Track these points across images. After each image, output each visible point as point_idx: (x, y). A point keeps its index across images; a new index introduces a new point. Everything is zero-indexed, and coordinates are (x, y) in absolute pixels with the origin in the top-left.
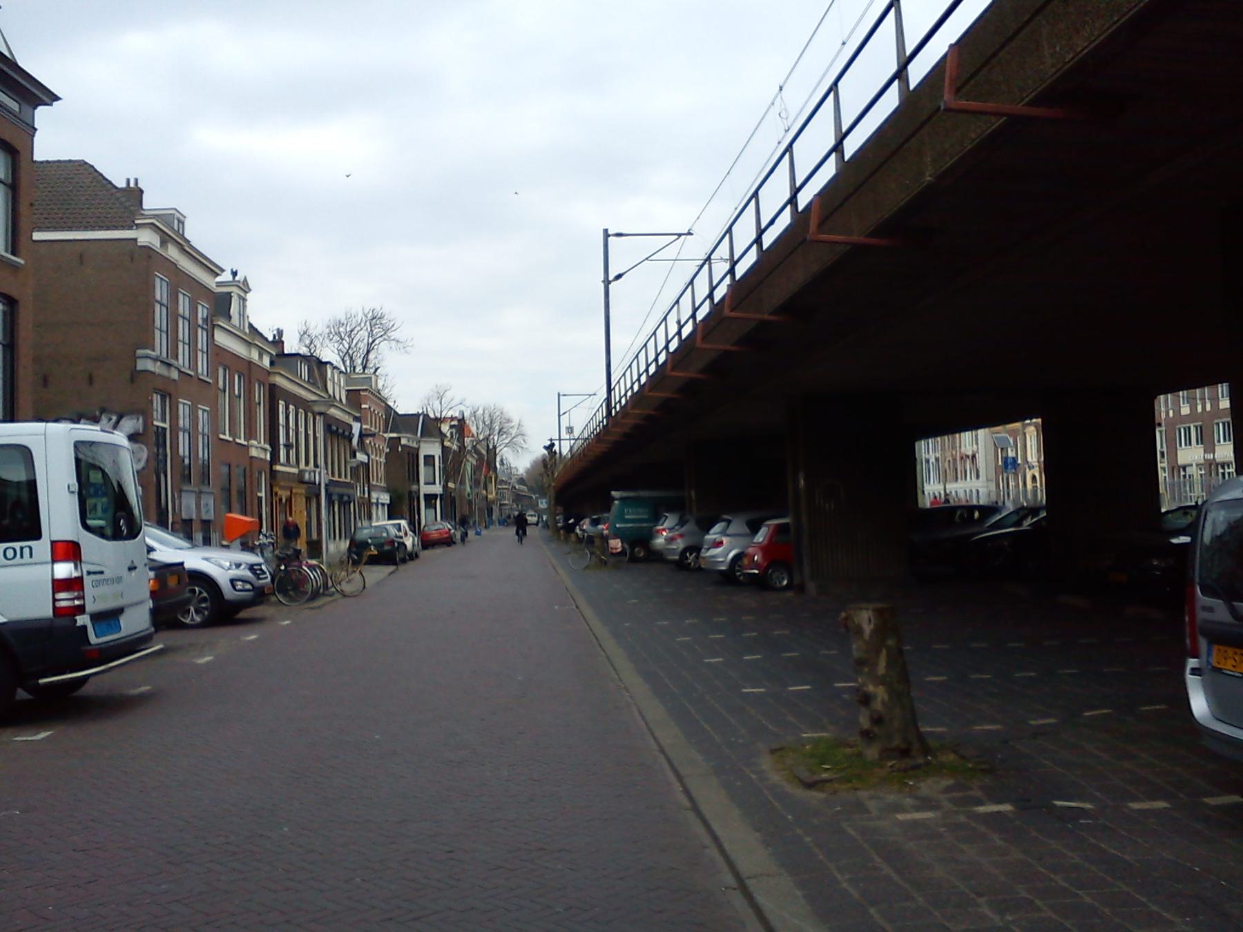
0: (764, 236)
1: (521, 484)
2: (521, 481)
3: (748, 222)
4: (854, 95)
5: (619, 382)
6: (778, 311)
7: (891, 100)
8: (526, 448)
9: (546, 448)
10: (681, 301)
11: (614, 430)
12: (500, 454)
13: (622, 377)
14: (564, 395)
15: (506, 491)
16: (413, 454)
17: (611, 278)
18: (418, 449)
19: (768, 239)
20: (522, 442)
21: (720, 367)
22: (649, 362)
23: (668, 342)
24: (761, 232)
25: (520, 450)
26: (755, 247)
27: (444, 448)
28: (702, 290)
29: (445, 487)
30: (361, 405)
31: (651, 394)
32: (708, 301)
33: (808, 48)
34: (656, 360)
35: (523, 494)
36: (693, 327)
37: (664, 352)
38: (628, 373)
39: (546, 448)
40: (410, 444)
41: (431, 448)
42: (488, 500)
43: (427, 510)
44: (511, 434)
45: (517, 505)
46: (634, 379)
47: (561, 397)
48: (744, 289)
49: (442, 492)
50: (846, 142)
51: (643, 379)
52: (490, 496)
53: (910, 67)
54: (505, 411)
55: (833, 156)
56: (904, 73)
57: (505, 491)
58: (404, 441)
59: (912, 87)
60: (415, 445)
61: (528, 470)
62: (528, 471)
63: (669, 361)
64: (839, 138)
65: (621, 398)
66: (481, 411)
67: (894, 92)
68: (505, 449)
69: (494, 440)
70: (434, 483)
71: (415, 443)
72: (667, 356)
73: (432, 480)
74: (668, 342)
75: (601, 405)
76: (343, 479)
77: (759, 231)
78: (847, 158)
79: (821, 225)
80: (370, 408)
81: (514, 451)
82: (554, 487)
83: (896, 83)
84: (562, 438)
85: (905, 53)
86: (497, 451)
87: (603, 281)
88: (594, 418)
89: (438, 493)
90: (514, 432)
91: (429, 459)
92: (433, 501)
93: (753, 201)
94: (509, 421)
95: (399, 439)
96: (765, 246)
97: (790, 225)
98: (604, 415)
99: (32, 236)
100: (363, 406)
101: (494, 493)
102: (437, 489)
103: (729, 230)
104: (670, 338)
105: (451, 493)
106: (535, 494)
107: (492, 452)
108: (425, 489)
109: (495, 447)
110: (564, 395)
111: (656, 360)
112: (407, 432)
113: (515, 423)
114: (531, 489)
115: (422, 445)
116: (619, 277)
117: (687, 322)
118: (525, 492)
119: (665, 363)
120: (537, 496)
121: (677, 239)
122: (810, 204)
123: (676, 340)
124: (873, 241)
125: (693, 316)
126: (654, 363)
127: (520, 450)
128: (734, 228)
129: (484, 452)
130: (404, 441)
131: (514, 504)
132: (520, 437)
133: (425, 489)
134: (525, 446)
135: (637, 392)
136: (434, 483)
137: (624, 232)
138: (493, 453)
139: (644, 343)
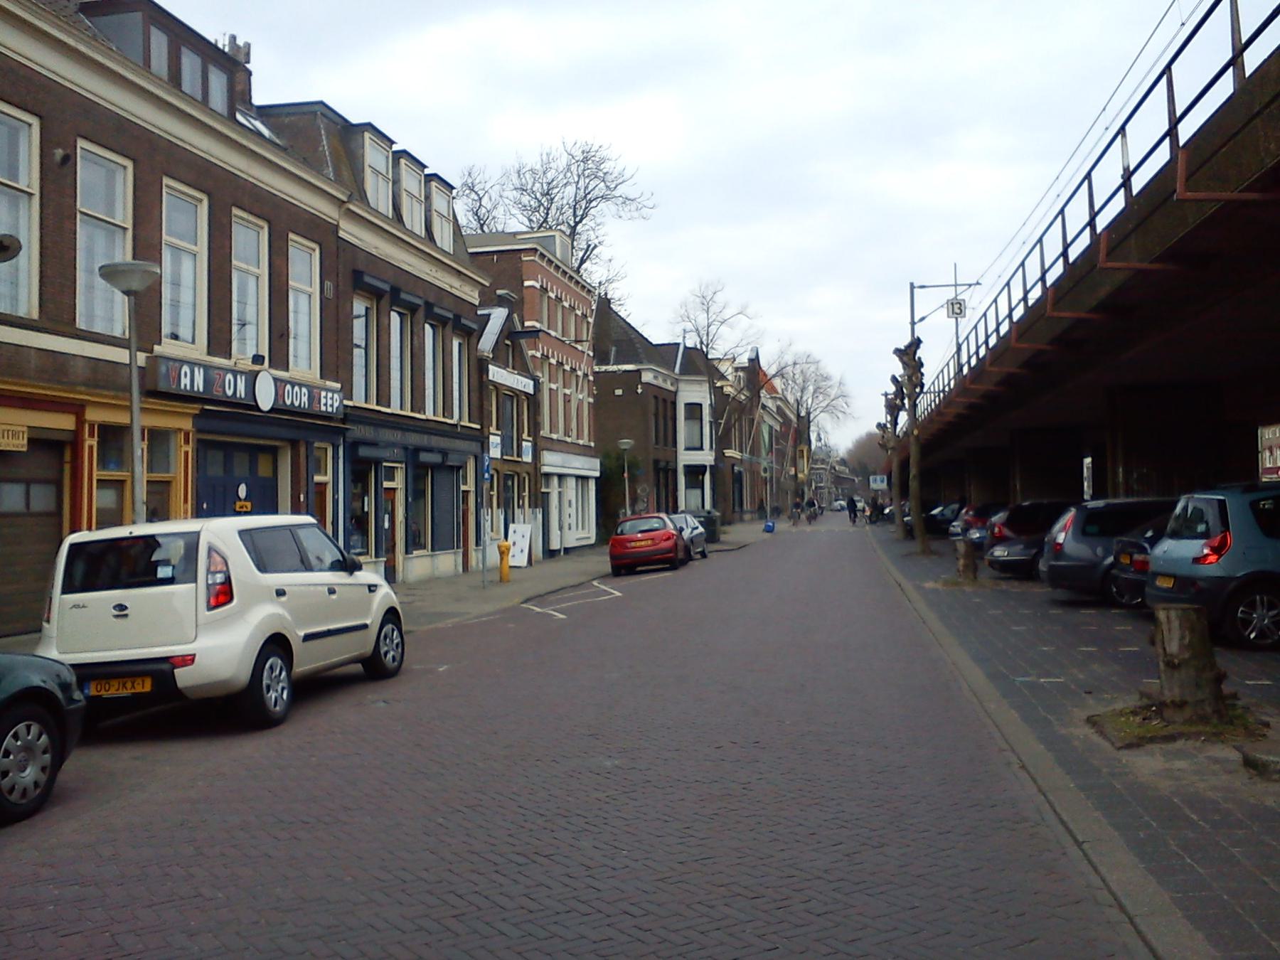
0: (1134, 179)
1: (841, 465)
2: (843, 462)
4: (1187, 81)
5: (967, 338)
6: (1094, 310)
7: (1225, 87)
8: (850, 414)
9: (898, 352)
10: (1128, 127)
11: (958, 400)
12: (816, 421)
16: (666, 402)
17: (916, 320)
18: (676, 393)
19: (1102, 222)
20: (844, 405)
21: (1034, 363)
22: (989, 333)
23: (998, 325)
25: (840, 415)
27: (717, 392)
28: (1033, 272)
29: (720, 456)
30: (523, 283)
31: (973, 386)
32: (1061, 260)
34: (997, 330)
35: (845, 476)
37: (1007, 320)
39: (898, 352)
40: (660, 382)
41: (694, 392)
42: (799, 481)
43: (688, 491)
44: (829, 396)
45: (837, 488)
46: (972, 353)
48: (1059, 294)
49: (713, 463)
50: (1180, 127)
51: (982, 352)
52: (800, 475)
53: (1246, 54)
56: (1240, 60)
57: (821, 471)
58: (647, 377)
59: (1248, 74)
60: (668, 386)
61: (850, 450)
62: (850, 452)
63: (988, 356)
64: (1126, 176)
67: (1228, 79)
68: (822, 414)
69: (807, 404)
70: (701, 448)
71: (669, 383)
72: (986, 351)
73: (698, 445)
74: (998, 325)
75: (948, 364)
76: (395, 408)
77: (1093, 214)
78: (1135, 192)
79: (1017, 340)
80: (544, 290)
81: (833, 418)
82: (917, 437)
83: (1231, 70)
84: (954, 283)
85: (1240, 40)
86: (812, 416)
87: (910, 323)
89: (707, 464)
90: (833, 392)
91: (694, 410)
92: (701, 477)
93: (1086, 183)
94: (827, 378)
95: (638, 372)
98: (952, 375)
99: (623, 392)
100: (527, 283)
101: (806, 472)
102: (706, 457)
104: (1000, 320)
105: (733, 466)
106: (857, 477)
107: (805, 422)
108: (686, 458)
109: (808, 414)
111: (997, 330)
112: (650, 362)
113: (835, 381)
114: (853, 471)
115: (682, 386)
116: (922, 319)
117: (992, 334)
118: (846, 474)
119: (984, 357)
121: (968, 288)
123: (1007, 323)
125: (1025, 299)
126: (995, 334)
127: (840, 415)
128: (1093, 174)
129: (793, 417)
130: (647, 377)
131: (833, 486)
132: (840, 399)
133: (686, 458)
134: (848, 411)
136: (701, 448)
138: (805, 420)
139: (946, 362)
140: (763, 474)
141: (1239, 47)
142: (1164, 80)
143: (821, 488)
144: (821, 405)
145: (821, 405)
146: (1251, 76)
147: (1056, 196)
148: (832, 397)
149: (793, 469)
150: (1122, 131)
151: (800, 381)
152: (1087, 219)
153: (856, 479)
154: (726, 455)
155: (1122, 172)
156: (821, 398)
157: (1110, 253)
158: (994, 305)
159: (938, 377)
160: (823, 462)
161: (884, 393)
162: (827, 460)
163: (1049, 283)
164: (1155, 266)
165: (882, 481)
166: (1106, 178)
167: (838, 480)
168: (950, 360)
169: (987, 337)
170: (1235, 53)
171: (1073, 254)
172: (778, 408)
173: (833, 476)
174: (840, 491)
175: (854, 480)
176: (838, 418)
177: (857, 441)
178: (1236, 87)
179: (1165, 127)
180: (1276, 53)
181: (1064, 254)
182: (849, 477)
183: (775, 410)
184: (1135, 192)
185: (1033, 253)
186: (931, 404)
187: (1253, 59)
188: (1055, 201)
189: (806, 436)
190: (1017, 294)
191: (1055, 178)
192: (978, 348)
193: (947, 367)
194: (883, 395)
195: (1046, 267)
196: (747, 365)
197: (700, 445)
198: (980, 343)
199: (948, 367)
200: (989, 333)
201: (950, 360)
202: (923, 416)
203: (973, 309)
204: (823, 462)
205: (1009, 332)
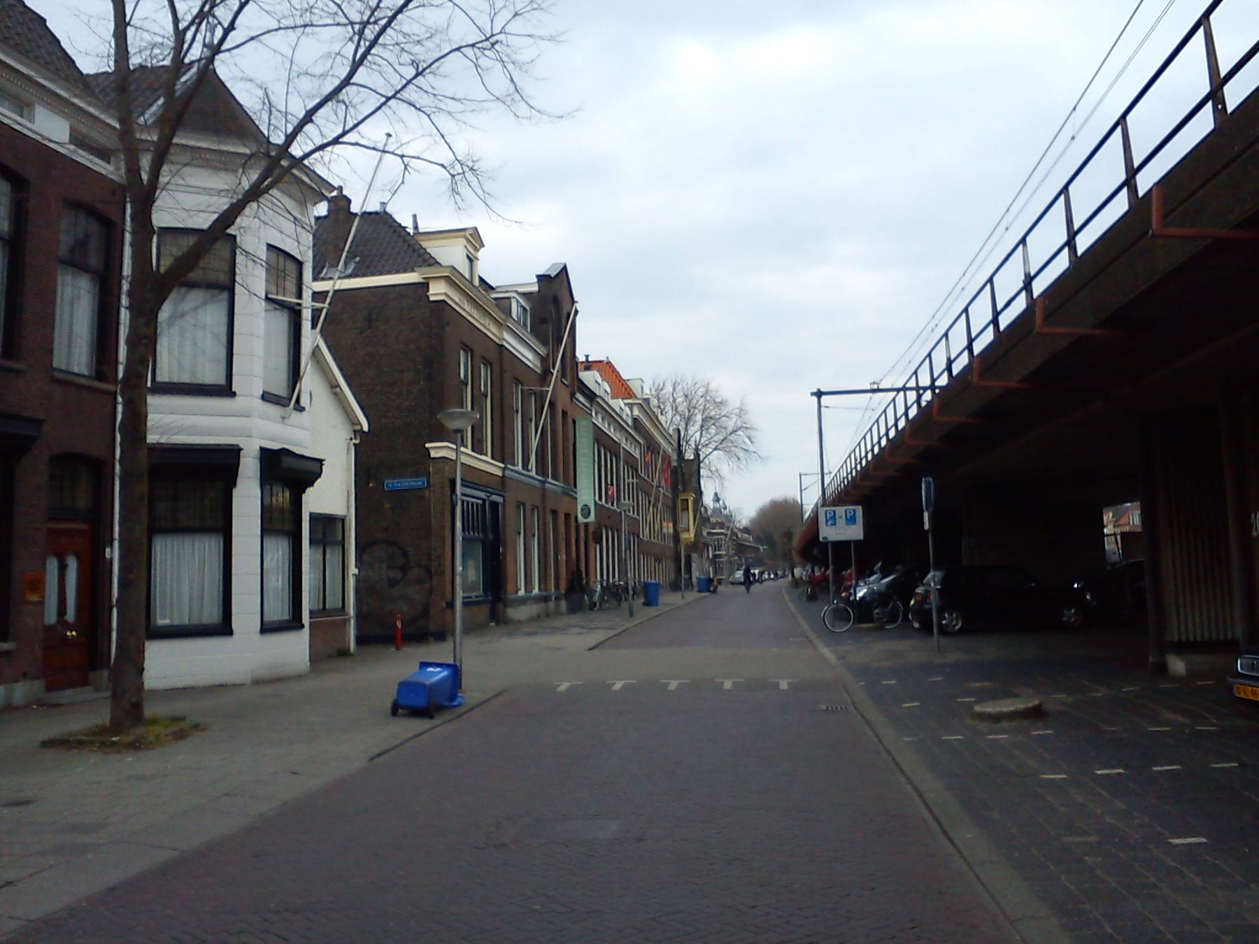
0: (1079, 239)
2: (746, 530)
3: (984, 302)
4: (1084, 199)
12: (706, 461)
13: (881, 414)
14: (805, 475)
15: (723, 537)
20: (747, 440)
24: (996, 314)
25: (741, 454)
26: (991, 327)
33: (1051, 141)
36: (969, 360)
38: (868, 436)
45: (740, 558)
46: (857, 462)
47: (802, 477)
51: (902, 424)
53: (1226, 88)
54: (712, 387)
55: (1125, 190)
57: (720, 537)
62: (753, 521)
63: (907, 428)
65: (861, 459)
66: (669, 389)
68: (715, 452)
74: (907, 409)
77: (970, 341)
78: (1080, 252)
79: (981, 376)
88: (833, 482)
96: (1002, 327)
97: (1068, 269)
103: (990, 280)
106: (762, 545)
110: (805, 475)
116: (805, 489)
117: (912, 405)
118: (750, 542)
119: (904, 429)
120: (765, 547)
122: (1150, 191)
123: (893, 429)
124: (1097, 332)
127: (741, 454)
132: (740, 432)
134: (752, 448)
135: (865, 467)
137: (808, 473)
140: (581, 519)
141: (1072, 233)
142: (1062, 198)
143: (720, 556)
144: (715, 439)
145: (715, 439)
146: (1233, 112)
147: (1009, 229)
148: (730, 429)
149: (671, 525)
150: (1065, 191)
151: (683, 408)
152: (1064, 238)
153: (761, 548)
154: (433, 454)
155: (1023, 278)
156: (713, 431)
157: (1047, 318)
158: (927, 361)
159: (846, 461)
160: (722, 525)
161: (815, 390)
162: (728, 525)
163: (976, 352)
164: (1097, 332)
165: (851, 520)
166: (1009, 282)
167: (741, 548)
168: (861, 440)
169: (897, 420)
170: (1220, 92)
171: (1005, 321)
172: (635, 420)
173: (735, 543)
174: (743, 561)
175: (759, 549)
176: (739, 459)
177: (761, 510)
178: (1072, 259)
179: (1122, 177)
180: (1121, 220)
181: (970, 348)
182: (753, 545)
183: (630, 423)
184: (1080, 252)
185: (983, 293)
186: (844, 480)
187: (1235, 95)
188: (960, 293)
189: (695, 485)
190: (939, 364)
191: (1071, 109)
192: (880, 439)
193: (863, 440)
194: (813, 394)
195: (1076, 227)
196: (535, 288)
197: (221, 380)
198: (889, 426)
199: (860, 448)
200: (898, 416)
201: (861, 440)
202: (842, 485)
203: (873, 410)
204: (722, 525)
205: (966, 370)
